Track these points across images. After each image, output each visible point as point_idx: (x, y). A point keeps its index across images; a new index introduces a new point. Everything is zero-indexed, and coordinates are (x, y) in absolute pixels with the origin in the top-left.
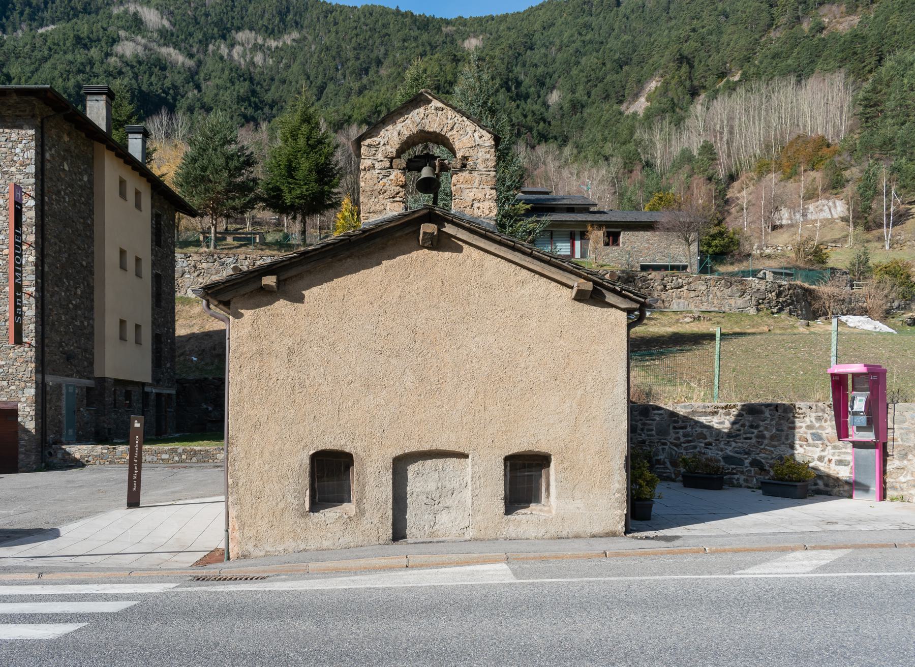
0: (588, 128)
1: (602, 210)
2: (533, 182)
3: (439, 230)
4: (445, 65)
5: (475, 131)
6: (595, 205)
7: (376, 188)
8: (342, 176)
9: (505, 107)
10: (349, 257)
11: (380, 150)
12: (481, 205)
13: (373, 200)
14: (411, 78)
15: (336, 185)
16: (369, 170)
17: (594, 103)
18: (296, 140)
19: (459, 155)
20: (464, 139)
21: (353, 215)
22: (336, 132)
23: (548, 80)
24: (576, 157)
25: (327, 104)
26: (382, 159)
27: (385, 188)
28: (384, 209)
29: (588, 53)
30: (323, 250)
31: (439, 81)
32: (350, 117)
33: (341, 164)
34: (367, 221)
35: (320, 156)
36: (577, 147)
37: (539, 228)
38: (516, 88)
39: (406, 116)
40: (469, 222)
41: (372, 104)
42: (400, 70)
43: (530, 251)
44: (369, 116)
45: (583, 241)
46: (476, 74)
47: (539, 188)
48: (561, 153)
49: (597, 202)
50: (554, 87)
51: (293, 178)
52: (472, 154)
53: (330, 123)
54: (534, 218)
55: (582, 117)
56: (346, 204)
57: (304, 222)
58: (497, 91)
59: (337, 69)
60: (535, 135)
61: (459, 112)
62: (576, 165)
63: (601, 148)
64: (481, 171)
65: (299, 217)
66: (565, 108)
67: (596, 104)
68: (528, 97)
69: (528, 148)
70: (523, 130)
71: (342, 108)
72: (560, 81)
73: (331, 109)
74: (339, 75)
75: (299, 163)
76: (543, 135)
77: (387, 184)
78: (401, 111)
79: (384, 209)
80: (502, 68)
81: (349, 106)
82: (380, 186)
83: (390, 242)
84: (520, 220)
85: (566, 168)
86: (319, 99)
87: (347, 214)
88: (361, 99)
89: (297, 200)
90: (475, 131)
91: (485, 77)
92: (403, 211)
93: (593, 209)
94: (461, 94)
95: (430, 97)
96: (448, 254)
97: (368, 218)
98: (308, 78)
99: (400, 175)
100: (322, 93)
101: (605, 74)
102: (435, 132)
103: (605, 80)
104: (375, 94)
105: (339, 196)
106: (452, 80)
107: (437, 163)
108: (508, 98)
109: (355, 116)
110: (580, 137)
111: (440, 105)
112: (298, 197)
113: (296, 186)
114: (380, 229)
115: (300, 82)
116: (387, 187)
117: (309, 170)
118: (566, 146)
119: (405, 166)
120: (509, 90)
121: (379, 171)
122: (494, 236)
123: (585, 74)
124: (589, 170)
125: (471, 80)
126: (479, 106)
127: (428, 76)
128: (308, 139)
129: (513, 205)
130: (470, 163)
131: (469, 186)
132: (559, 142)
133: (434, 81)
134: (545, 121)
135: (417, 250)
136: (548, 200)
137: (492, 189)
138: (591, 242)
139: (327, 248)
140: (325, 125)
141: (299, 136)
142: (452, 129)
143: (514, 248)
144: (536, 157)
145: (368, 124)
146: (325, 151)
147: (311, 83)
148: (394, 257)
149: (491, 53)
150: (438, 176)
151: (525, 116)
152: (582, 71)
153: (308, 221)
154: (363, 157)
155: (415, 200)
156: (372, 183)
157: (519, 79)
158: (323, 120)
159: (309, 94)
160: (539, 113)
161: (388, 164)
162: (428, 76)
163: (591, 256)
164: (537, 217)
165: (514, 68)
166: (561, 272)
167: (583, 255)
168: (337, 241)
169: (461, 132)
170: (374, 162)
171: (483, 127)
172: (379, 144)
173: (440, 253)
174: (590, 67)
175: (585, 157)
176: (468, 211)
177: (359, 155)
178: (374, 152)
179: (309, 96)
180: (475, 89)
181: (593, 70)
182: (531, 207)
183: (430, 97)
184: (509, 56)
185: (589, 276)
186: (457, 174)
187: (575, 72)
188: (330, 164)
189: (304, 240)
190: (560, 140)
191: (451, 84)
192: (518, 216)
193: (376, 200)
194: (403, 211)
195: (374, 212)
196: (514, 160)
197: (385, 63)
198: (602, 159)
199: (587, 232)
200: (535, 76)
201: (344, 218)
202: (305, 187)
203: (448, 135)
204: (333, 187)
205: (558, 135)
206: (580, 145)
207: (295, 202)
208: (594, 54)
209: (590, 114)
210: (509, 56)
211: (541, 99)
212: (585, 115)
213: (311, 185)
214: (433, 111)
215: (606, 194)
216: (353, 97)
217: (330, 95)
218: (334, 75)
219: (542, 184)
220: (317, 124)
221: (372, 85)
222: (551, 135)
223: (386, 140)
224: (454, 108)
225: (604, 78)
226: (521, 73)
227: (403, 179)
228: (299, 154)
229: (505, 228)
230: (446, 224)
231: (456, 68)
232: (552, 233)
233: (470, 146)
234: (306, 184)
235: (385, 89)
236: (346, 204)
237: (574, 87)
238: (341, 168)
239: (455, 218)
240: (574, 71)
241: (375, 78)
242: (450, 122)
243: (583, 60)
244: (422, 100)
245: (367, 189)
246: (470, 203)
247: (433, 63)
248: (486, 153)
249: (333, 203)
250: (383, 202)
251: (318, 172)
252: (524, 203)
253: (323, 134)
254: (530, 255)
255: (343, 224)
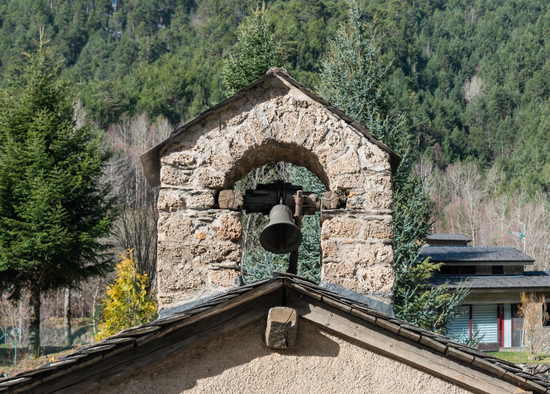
0: (520, 140)
1: (540, 269)
2: (443, 225)
3: (300, 318)
4: (305, 21)
5: (360, 145)
6: (531, 262)
7: (186, 243)
8: (116, 213)
9: (402, 100)
10: (132, 376)
11: (196, 173)
12: (368, 272)
13: (181, 266)
14: (249, 40)
15: (106, 231)
16: (174, 210)
17: (528, 101)
18: (22, 140)
19: (334, 185)
20: (343, 158)
21: (138, 290)
22: (105, 127)
23: (465, 60)
24: (504, 184)
25: (87, 74)
26: (200, 189)
27: (204, 243)
28: (203, 283)
29: (520, 23)
30: (82, 365)
31: (295, 46)
32: (133, 101)
33: (116, 190)
34: (169, 306)
35: (74, 173)
36: (506, 170)
37: (453, 302)
38: (418, 70)
39: (244, 114)
40: (350, 302)
41: (175, 78)
42: (228, 21)
43: (444, 347)
44: (171, 102)
45: (515, 320)
46: (358, 43)
47: (452, 235)
48: (484, 178)
49: (533, 257)
50: (473, 73)
51: (15, 216)
52: (354, 184)
53: (94, 110)
54: (446, 286)
55: (513, 122)
56: (126, 269)
57: (36, 303)
58: (390, 72)
59: (109, 9)
60: (446, 147)
61: (334, 111)
62: (504, 198)
63: (539, 171)
64: (369, 213)
65: (26, 295)
66: (488, 107)
67: (531, 104)
68: (436, 86)
69: (437, 169)
70: (428, 138)
71: (119, 83)
72: (482, 63)
73: (96, 83)
74: (114, 20)
75: (28, 188)
76: (458, 148)
77: (208, 237)
78: (236, 104)
79: (203, 283)
80: (397, 35)
81: (131, 81)
82: (194, 240)
83: (212, 344)
84: (424, 290)
85: (491, 203)
86: (71, 63)
87: (126, 288)
88: (155, 69)
89: (22, 261)
90: (360, 145)
91: (373, 48)
92: (237, 286)
93: (529, 268)
94: (334, 74)
95: (286, 83)
96: (314, 360)
97: (171, 300)
98: (51, 20)
99: (231, 219)
100: (77, 50)
101: (544, 59)
102: (294, 145)
103: (544, 68)
104: (183, 62)
105: (110, 251)
106: (318, 47)
107: (297, 199)
108: (406, 86)
109: (143, 100)
110: (510, 154)
111: (302, 97)
112: (23, 255)
113: (20, 233)
114: (194, 320)
115: (33, 27)
116: (208, 241)
117: (49, 203)
118: (490, 166)
119: (240, 203)
120: (407, 71)
121: (193, 213)
122: (389, 324)
123: (516, 56)
124: (523, 206)
125: (350, 52)
126: (362, 97)
127: (278, 38)
128: (49, 140)
129: (415, 265)
130: (352, 199)
131: (350, 240)
132: (480, 160)
133: (288, 46)
134: (460, 126)
135: (262, 355)
136: (466, 254)
137: (386, 244)
138: (526, 322)
139: (89, 362)
140: (84, 114)
141: (29, 133)
142: (323, 139)
143: (419, 344)
144: (448, 184)
145: (174, 119)
146: (85, 164)
147: (57, 30)
148: (219, 372)
149: (380, 8)
150: (298, 221)
151: (432, 116)
152: (512, 50)
153: (44, 302)
154: (163, 185)
155: (254, 259)
156: (179, 233)
157: (423, 55)
158: (79, 105)
159: (49, 51)
160: (452, 111)
161: (210, 200)
162: (278, 38)
163: (526, 342)
164: (450, 283)
165: (415, 36)
166: (489, 378)
167: (515, 342)
168: (110, 347)
169: (337, 147)
170: (184, 195)
171: (373, 138)
172: (194, 162)
173: (301, 358)
174: (524, 44)
175: (517, 186)
176: (348, 283)
177: (155, 182)
178: (184, 177)
179: (51, 57)
180: (355, 67)
181: (527, 50)
182: (442, 268)
183: (286, 83)
184: (407, 16)
185: (529, 382)
186: (330, 218)
187: (503, 51)
188: (91, 190)
189: (36, 341)
190: (481, 157)
191: (316, 54)
192: (422, 282)
193: (188, 266)
194: (237, 286)
195: (184, 289)
196: (416, 190)
197: (201, 6)
198: (541, 189)
199: (521, 305)
200: (446, 52)
201: (121, 296)
202: (40, 235)
203: (316, 150)
204: (99, 234)
205: (479, 149)
206: (510, 167)
207: (17, 264)
208: (529, 25)
209: (523, 118)
210: (407, 16)
211: (455, 90)
212: (517, 119)
213: (52, 231)
214: (291, 108)
215: (546, 244)
216: (141, 64)
217: (94, 57)
218: (103, 19)
219: (456, 228)
220: (69, 112)
221: (177, 44)
222: (469, 149)
223: (207, 155)
224: (327, 105)
225: (541, 64)
226: (425, 45)
227: (237, 227)
228: (29, 171)
229: (402, 304)
230: (311, 306)
231: (323, 28)
232: (471, 307)
233: (352, 170)
234: (41, 229)
235: (201, 53)
236: (126, 269)
237: (501, 74)
238: (116, 198)
239: (328, 296)
240: (502, 50)
241: (183, 33)
242: (319, 127)
243: (514, 34)
244: (273, 87)
245: (171, 246)
246: (351, 269)
247: (286, 14)
248: (377, 182)
249: (98, 265)
250: (200, 269)
251: (67, 205)
252: (430, 261)
253: (80, 132)
254: (444, 354)
255: (118, 309)
